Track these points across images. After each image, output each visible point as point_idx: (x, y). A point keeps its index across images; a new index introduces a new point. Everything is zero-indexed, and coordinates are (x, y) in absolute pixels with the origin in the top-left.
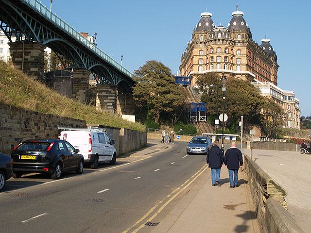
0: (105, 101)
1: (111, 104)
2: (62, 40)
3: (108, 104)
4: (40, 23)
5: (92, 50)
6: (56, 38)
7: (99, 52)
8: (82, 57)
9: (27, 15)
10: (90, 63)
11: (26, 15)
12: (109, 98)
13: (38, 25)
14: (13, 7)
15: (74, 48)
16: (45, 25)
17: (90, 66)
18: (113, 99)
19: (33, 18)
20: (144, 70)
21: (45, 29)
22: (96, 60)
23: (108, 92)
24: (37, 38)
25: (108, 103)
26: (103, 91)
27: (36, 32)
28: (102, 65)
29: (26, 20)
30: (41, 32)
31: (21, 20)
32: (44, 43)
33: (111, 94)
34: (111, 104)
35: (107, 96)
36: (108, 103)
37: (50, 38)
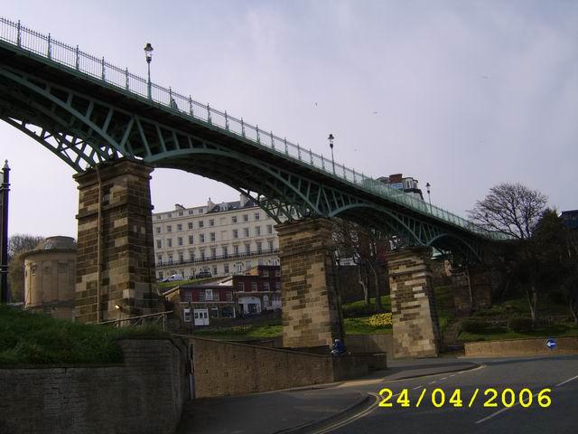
0: (407, 283)
1: (420, 288)
2: (366, 205)
3: (414, 289)
4: (85, 97)
5: (513, 240)
6: (182, 147)
7: (434, 210)
8: (412, 227)
9: (291, 174)
10: (428, 234)
11: (287, 175)
12: (414, 276)
13: (314, 188)
14: (262, 167)
15: (392, 215)
16: (316, 181)
17: (429, 240)
18: (423, 277)
19: (293, 174)
20: (489, 206)
21: (329, 193)
22: (349, 196)
23: (409, 264)
24: (419, 240)
25: (414, 286)
26: (399, 264)
27: (417, 232)
28: (373, 206)
29: (403, 223)
30: (322, 198)
31: (294, 195)
32: (428, 243)
33: (417, 268)
34: (420, 288)
35: (410, 274)
36: (414, 286)
37: (433, 236)
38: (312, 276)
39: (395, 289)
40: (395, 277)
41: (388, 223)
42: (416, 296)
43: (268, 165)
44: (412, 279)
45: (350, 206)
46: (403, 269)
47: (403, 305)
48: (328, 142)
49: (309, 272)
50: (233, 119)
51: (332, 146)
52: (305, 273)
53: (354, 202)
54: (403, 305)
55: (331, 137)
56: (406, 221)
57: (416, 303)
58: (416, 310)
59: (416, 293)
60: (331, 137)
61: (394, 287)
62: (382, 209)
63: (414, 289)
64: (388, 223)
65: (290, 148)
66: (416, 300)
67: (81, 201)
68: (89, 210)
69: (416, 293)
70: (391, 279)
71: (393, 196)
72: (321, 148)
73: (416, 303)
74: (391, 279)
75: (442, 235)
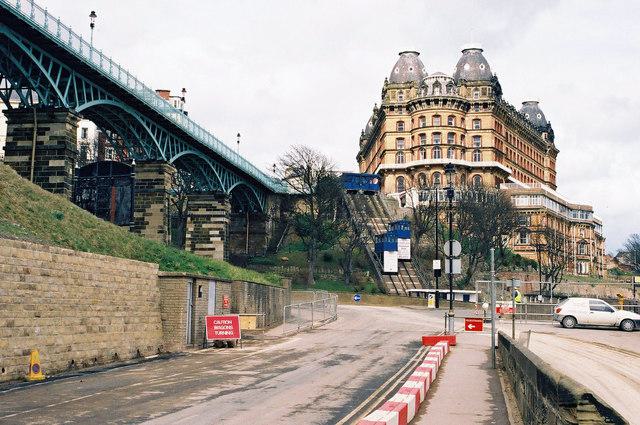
0: (204, 226)
1: (217, 232)
3: (211, 233)
7: (191, 126)
9: (43, 53)
12: (213, 219)
22: (99, 89)
23: (210, 208)
25: (211, 229)
26: (200, 206)
27: (62, 88)
32: (78, 109)
34: (217, 232)
35: (209, 217)
36: (211, 229)
37: (89, 100)
38: (151, 214)
39: (191, 229)
40: (193, 217)
41: (131, 127)
42: (211, 239)
43: (20, 37)
44: (210, 223)
45: (99, 102)
46: (202, 212)
47: (197, 246)
48: (89, 21)
49: (148, 211)
50: (39, 8)
51: (92, 25)
52: (143, 211)
53: (103, 98)
54: (197, 246)
55: (93, 14)
56: (46, 64)
57: (210, 246)
58: (211, 252)
59: (213, 236)
60: (93, 14)
61: (191, 228)
62: (130, 111)
63: (211, 233)
64: (131, 127)
65: (50, 21)
66: (211, 243)
67: (8, 135)
68: (19, 145)
69: (213, 236)
70: (189, 219)
71: (168, 115)
72: (231, 143)
73: (210, 246)
74: (189, 219)
75: (237, 184)
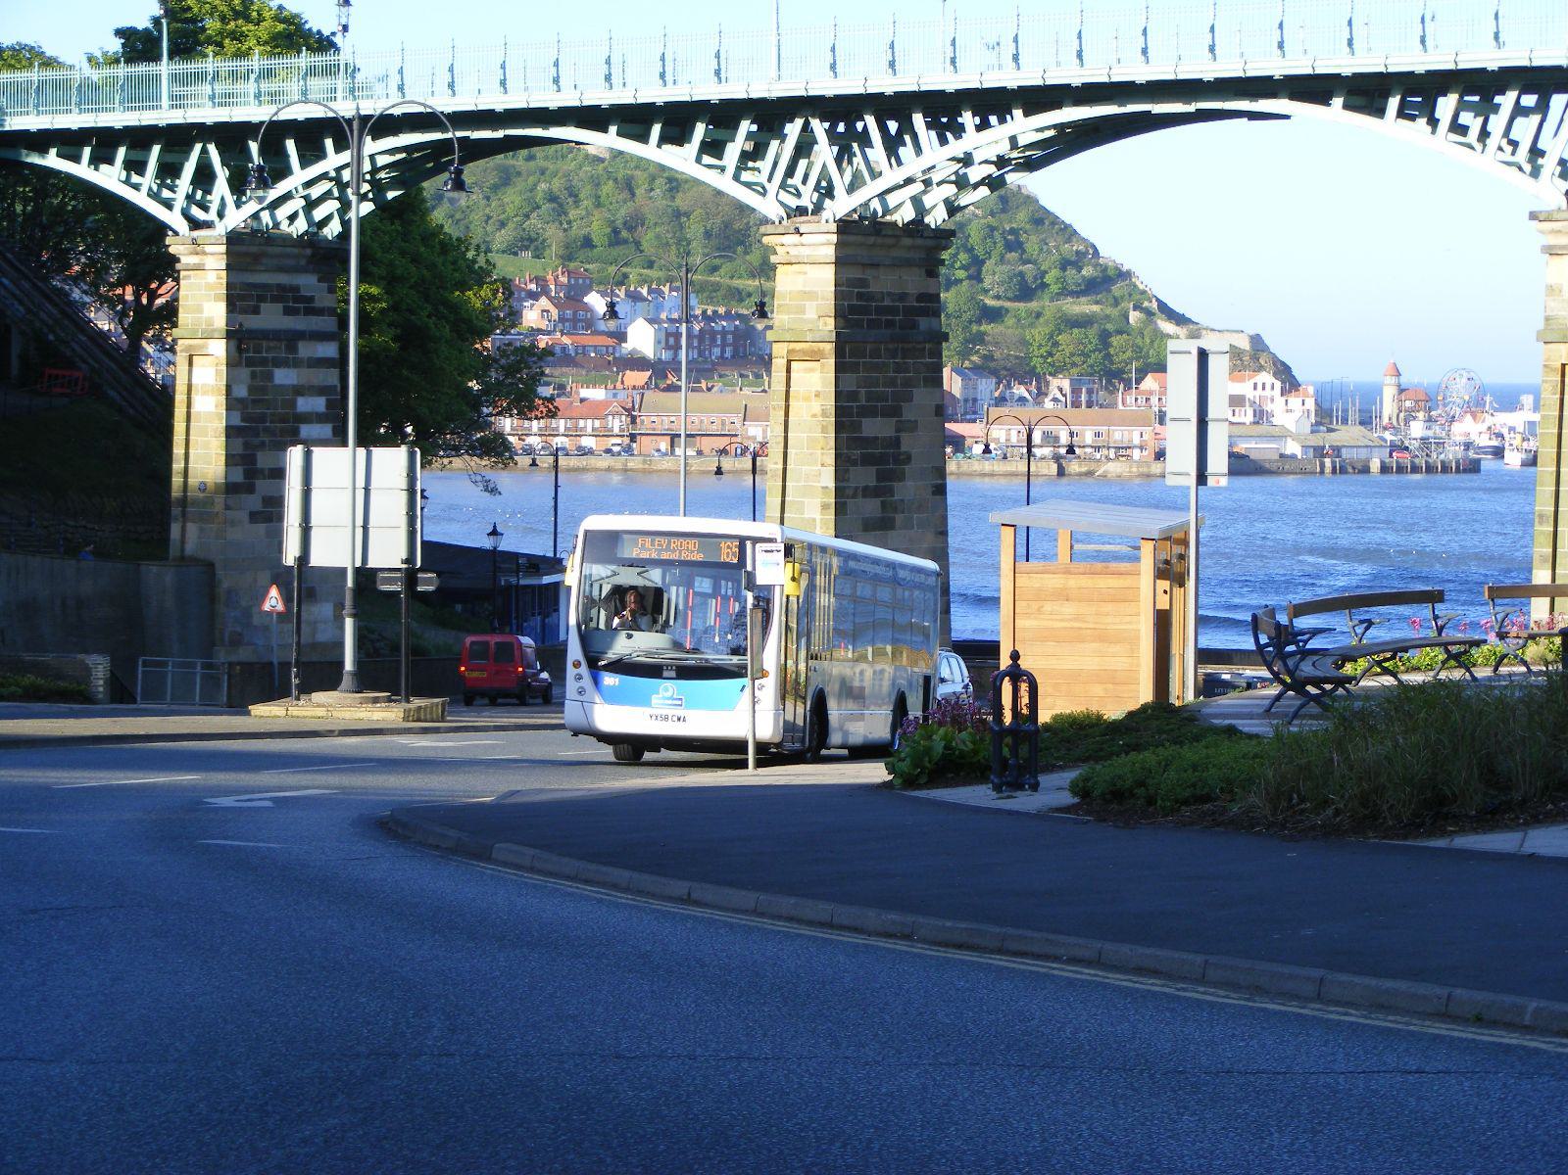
35: (293, 338)
36: (299, 391)
44: (296, 363)
